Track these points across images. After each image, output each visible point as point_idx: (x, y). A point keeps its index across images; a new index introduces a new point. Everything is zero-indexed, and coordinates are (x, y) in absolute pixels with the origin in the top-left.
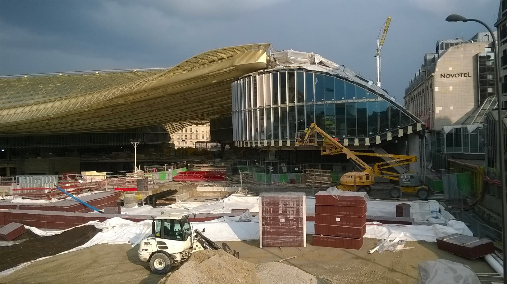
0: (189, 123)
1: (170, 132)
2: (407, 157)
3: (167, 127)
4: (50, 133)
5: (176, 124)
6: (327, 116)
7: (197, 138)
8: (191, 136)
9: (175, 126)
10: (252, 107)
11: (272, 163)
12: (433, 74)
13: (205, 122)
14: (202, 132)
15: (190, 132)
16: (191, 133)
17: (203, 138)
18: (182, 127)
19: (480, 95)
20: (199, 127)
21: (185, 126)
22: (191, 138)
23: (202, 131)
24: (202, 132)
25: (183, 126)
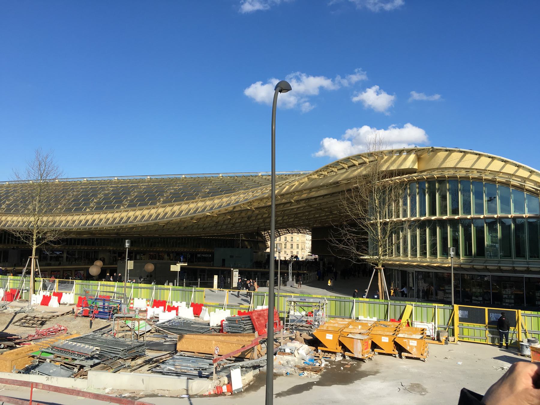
0: (286, 231)
1: (267, 239)
2: (168, 302)
3: (267, 235)
4: (534, 190)
5: (282, 230)
6: (43, 280)
7: (291, 248)
8: (285, 244)
9: (280, 232)
10: (387, 198)
11: (281, 271)
12: (118, 396)
13: (304, 230)
14: (296, 241)
15: (284, 241)
16: (286, 241)
17: (298, 248)
18: (278, 235)
19: (454, 277)
20: (294, 235)
21: (281, 234)
22: (285, 248)
23: (298, 241)
24: (296, 241)
25: (279, 234)
